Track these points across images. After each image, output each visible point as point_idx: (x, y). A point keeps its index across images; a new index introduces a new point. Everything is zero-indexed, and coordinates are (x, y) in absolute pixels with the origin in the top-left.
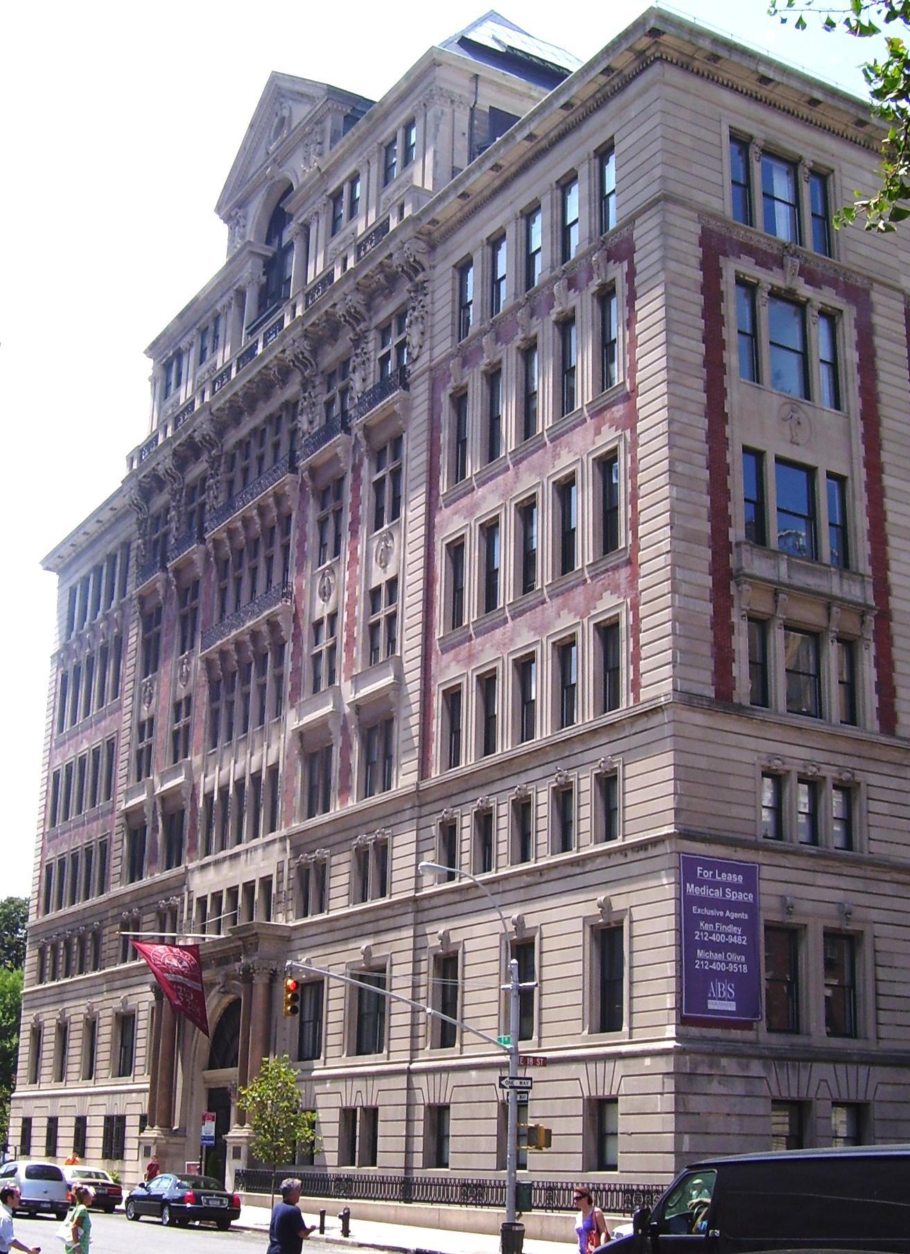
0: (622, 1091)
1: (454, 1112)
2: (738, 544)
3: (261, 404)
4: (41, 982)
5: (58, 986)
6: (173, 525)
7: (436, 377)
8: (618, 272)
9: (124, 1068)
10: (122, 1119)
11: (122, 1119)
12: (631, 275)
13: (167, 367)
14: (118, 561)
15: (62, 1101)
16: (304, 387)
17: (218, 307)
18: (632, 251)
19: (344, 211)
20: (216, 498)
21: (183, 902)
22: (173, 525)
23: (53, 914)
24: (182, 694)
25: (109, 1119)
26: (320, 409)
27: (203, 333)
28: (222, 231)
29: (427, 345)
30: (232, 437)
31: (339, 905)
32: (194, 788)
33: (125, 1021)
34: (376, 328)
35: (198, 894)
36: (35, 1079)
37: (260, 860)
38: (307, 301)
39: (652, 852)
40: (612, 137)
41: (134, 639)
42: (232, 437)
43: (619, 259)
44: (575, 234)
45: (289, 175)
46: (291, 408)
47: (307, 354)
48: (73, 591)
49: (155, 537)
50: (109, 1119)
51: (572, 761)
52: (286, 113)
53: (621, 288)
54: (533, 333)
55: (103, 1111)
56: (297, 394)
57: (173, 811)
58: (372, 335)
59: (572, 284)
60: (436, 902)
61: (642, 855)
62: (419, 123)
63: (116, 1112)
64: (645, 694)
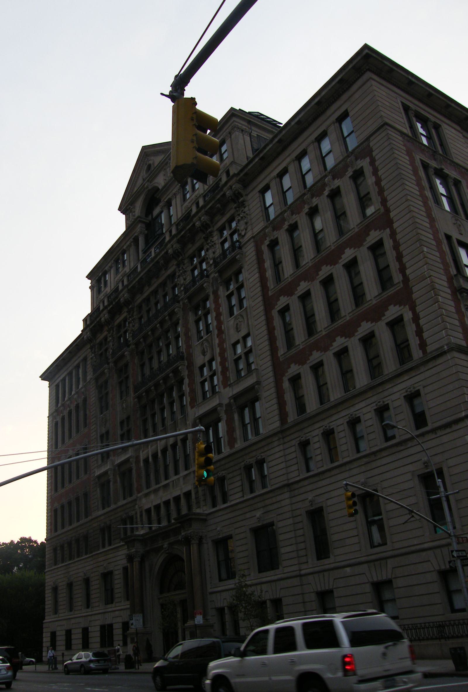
0: (334, 587)
1: (285, 601)
2: (455, 275)
3: (146, 288)
4: (55, 565)
5: (66, 565)
6: (111, 344)
7: (258, 239)
8: (365, 163)
9: (110, 599)
10: (111, 626)
11: (111, 626)
12: (373, 162)
13: (99, 281)
14: (67, 381)
15: (73, 621)
16: (178, 265)
17: (125, 247)
18: (371, 151)
19: (102, 285)
20: (134, 326)
21: (136, 513)
22: (111, 344)
23: (59, 532)
24: (104, 431)
25: (103, 627)
26: (189, 273)
27: (117, 261)
28: (122, 218)
29: (249, 228)
30: (139, 299)
31: (235, 498)
32: (137, 458)
33: (107, 576)
34: (217, 230)
35: (146, 507)
36: (56, 612)
37: (181, 485)
38: (128, 279)
39: (454, 427)
40: (347, 110)
41: (93, 399)
42: (139, 299)
43: (363, 158)
44: (271, 210)
45: (156, 185)
46: (173, 276)
47: (179, 250)
48: (57, 386)
49: (100, 352)
50: (103, 627)
51: (386, 393)
52: (151, 162)
53: (368, 171)
54: (314, 205)
55: (99, 623)
56: (175, 270)
57: (124, 471)
58: (215, 233)
59: (274, 229)
60: (301, 484)
61: (448, 430)
62: (228, 141)
63: (108, 622)
64: (429, 349)
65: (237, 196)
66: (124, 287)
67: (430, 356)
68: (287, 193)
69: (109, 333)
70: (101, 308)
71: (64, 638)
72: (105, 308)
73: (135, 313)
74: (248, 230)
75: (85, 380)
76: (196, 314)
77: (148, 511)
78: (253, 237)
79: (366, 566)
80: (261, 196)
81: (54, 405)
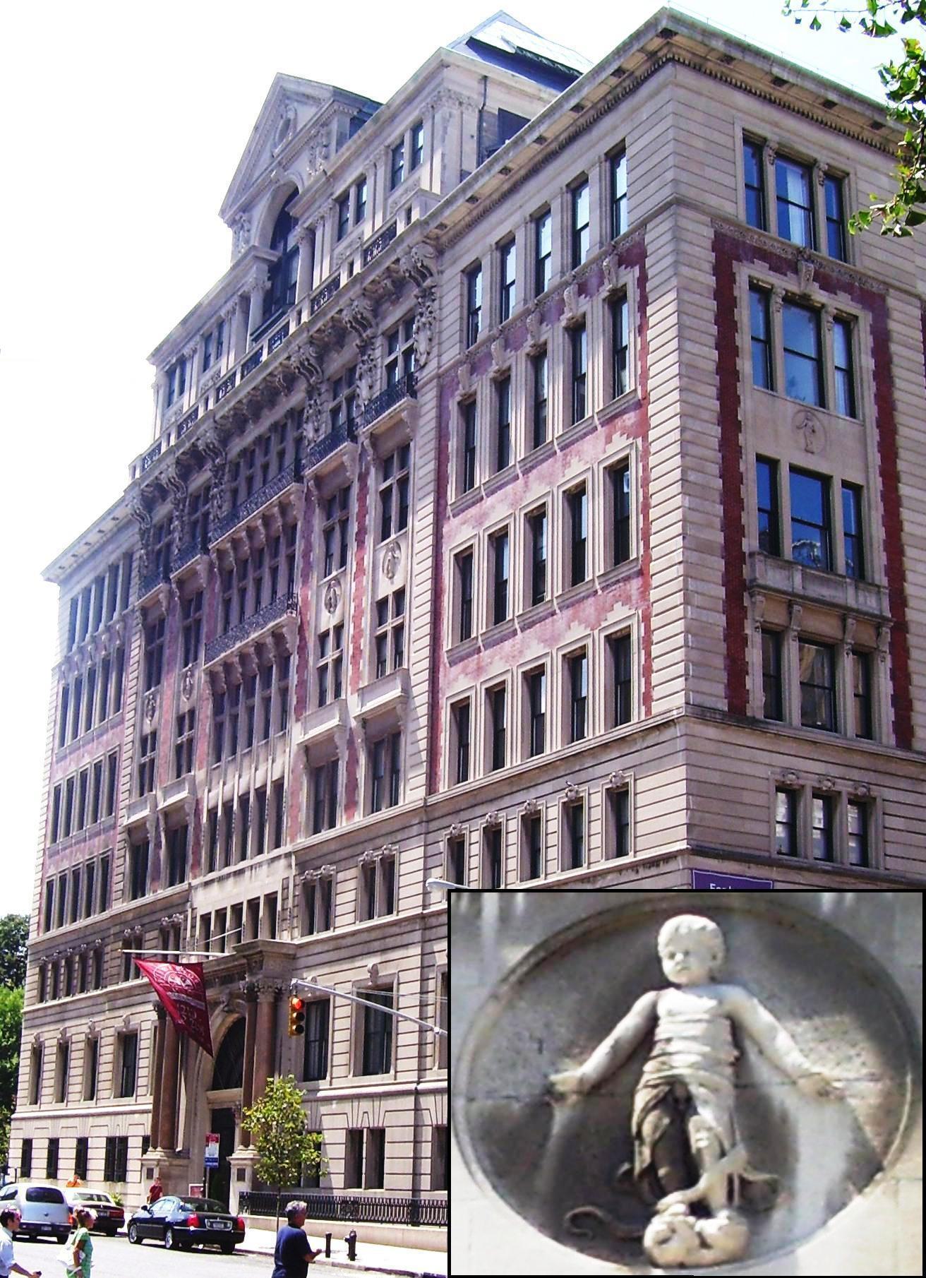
1: (388, 1136)
2: (752, 555)
3: (266, 412)
4: (41, 1001)
5: (60, 1005)
6: (176, 535)
7: (444, 384)
8: (629, 277)
9: (127, 1088)
10: (124, 1140)
11: (124, 1140)
12: (643, 280)
14: (121, 572)
16: (310, 394)
18: (643, 255)
19: (350, 215)
20: (220, 507)
21: (186, 920)
22: (176, 535)
24: (185, 708)
25: (111, 1141)
26: (326, 416)
27: (207, 339)
29: (435, 351)
33: (128, 1041)
34: (383, 334)
35: (201, 911)
36: (35, 1100)
37: (265, 876)
38: (312, 307)
40: (624, 140)
42: (237, 446)
43: (630, 264)
45: (295, 179)
46: (296, 416)
47: (312, 361)
48: (74, 603)
50: (111, 1141)
52: (291, 115)
53: (633, 294)
54: (542, 339)
57: (176, 827)
58: (379, 342)
59: (582, 290)
61: (654, 871)
63: (119, 1133)
64: (657, 708)
65: (423, 273)
66: (354, 280)
67: (659, 720)
68: (583, 233)
69: (215, 476)
70: (164, 449)
71: (73, 1154)
72: (171, 451)
73: (226, 478)
74: (432, 356)
75: (126, 604)
76: (329, 516)
77: (206, 918)
78: (439, 376)
79: (49, 1121)
80: (466, 282)
81: (65, 644)
